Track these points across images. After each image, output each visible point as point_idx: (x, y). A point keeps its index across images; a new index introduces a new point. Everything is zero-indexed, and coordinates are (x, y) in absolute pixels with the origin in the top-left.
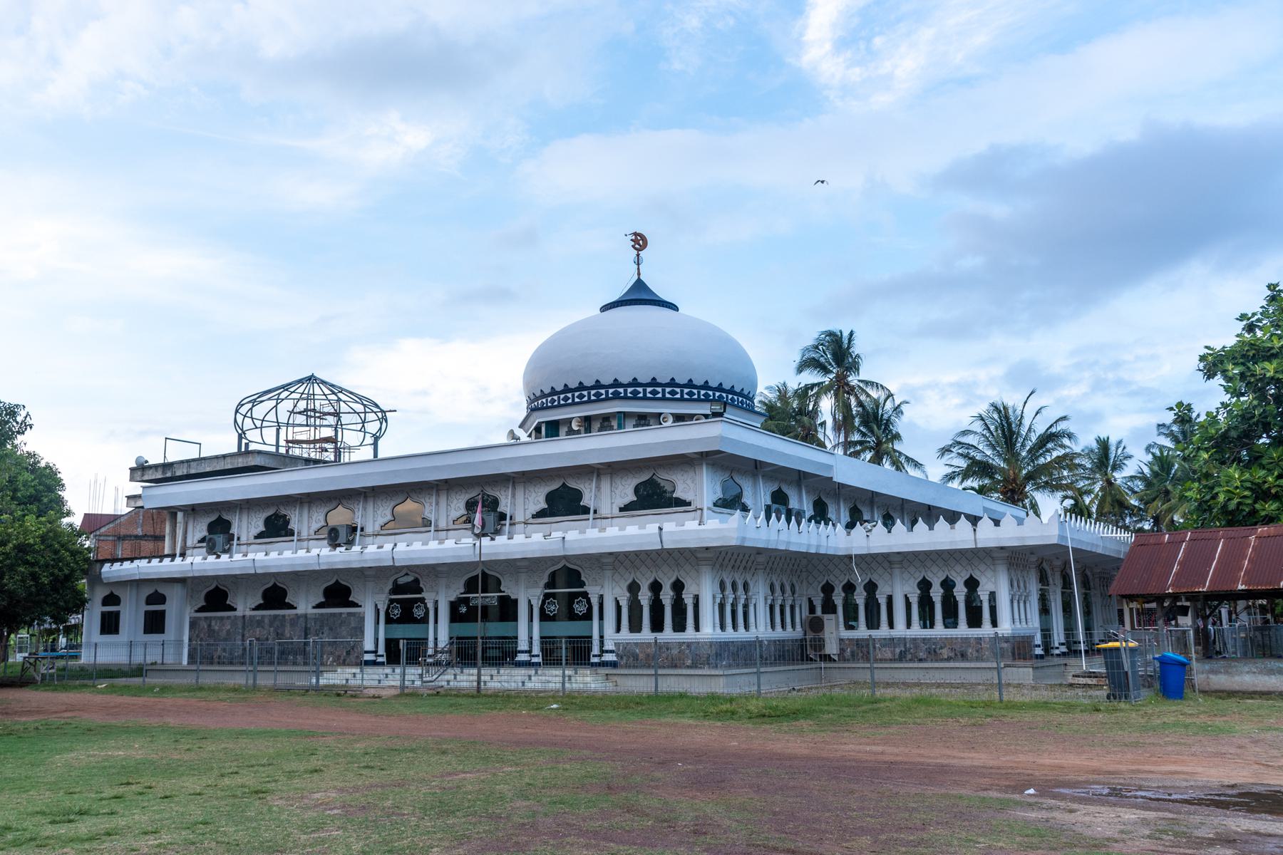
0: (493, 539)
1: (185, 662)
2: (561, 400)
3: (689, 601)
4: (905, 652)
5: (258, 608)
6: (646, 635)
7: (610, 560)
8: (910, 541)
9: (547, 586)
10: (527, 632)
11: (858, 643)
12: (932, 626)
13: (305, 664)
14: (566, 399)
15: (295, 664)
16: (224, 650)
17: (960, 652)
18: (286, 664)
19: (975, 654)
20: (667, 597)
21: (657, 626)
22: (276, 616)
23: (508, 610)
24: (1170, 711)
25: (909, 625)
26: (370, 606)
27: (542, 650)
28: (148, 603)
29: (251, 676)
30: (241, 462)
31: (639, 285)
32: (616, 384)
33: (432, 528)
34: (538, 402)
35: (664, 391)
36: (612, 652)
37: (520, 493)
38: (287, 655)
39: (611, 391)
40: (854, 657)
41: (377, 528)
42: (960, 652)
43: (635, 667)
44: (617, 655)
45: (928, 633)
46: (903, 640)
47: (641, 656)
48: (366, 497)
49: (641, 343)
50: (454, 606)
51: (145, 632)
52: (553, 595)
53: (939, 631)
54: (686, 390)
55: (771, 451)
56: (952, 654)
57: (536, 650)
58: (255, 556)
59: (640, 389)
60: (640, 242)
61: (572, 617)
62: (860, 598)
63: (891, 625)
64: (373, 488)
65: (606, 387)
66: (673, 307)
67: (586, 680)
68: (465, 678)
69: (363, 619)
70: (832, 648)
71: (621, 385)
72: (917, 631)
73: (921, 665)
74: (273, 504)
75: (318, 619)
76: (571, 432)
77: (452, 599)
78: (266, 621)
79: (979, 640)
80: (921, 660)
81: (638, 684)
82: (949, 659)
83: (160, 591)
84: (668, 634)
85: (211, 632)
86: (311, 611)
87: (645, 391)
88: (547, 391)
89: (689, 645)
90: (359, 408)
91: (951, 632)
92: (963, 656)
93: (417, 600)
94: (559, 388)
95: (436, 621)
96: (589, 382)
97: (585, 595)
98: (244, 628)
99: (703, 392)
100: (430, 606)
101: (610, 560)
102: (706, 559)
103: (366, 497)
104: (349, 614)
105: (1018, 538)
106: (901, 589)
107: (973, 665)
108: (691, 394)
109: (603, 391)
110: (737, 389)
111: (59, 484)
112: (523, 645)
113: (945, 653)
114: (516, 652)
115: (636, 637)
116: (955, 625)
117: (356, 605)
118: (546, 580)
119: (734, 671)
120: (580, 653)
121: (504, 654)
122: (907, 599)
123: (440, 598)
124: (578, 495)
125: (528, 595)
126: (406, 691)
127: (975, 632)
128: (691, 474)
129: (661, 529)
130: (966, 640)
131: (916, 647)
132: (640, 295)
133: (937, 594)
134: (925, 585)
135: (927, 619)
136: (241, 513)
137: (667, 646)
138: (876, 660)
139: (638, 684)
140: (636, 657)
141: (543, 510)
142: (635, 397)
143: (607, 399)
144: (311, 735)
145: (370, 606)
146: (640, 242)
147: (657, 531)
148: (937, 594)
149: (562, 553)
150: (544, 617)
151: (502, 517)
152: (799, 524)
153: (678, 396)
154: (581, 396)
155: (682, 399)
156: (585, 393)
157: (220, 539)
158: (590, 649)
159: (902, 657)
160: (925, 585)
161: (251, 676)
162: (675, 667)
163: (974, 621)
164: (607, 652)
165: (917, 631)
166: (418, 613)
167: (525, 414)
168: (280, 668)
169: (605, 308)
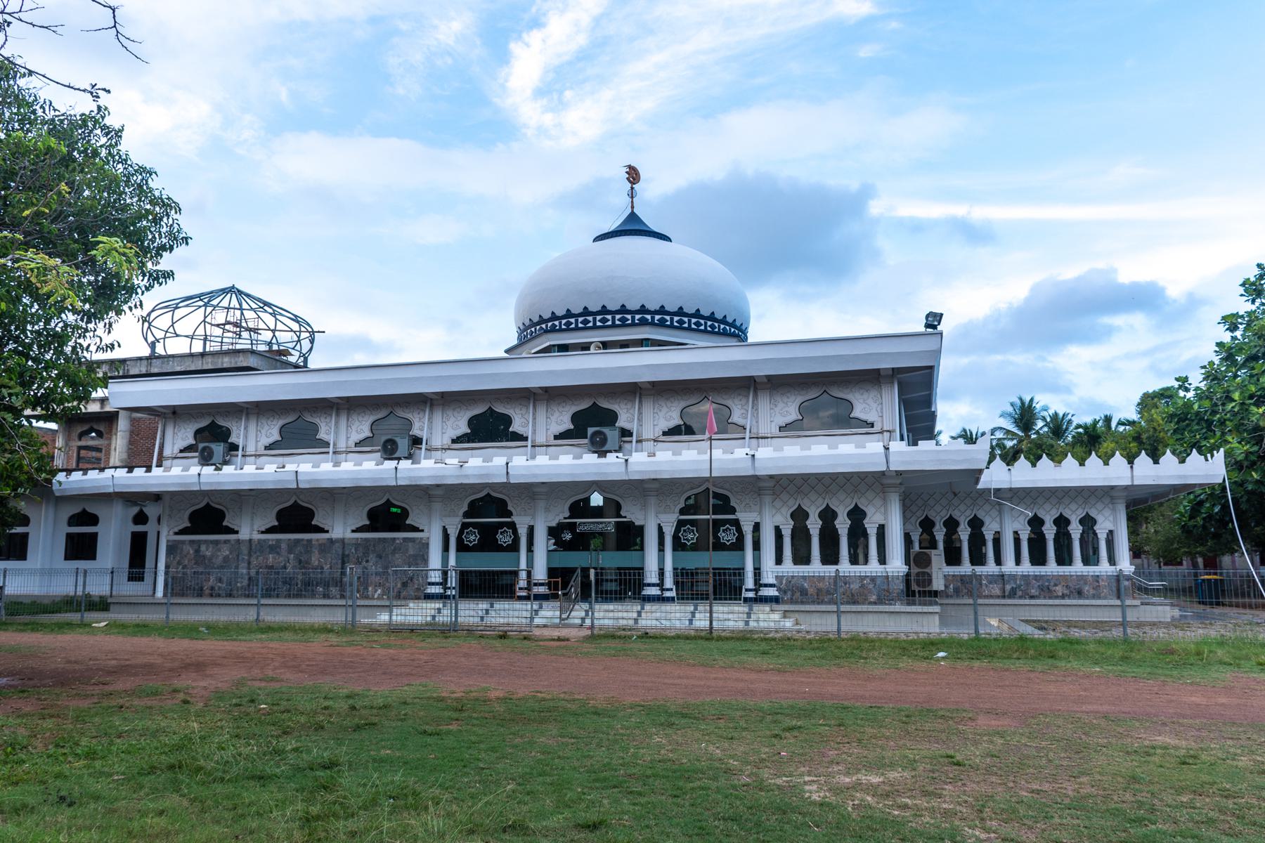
0: (217, 469)
1: (160, 593)
2: (548, 327)
3: (989, 537)
4: (1013, 590)
5: (270, 530)
6: (816, 567)
7: (771, 484)
8: (1058, 477)
10: (656, 562)
11: (963, 579)
12: (866, 562)
13: (343, 597)
15: (326, 596)
16: (220, 580)
17: (1077, 589)
18: (313, 596)
19: (1092, 592)
20: (1075, 530)
22: (298, 541)
23: (630, 537)
25: (1018, 562)
26: (434, 530)
27: (676, 583)
28: (70, 524)
29: (350, 610)
30: (226, 362)
31: (633, 217)
32: (643, 310)
33: (331, 450)
36: (654, 585)
37: (438, 416)
38: (304, 586)
39: (637, 317)
40: (957, 592)
41: (176, 450)
42: (1077, 589)
43: (802, 603)
44: (779, 590)
46: (1013, 577)
47: (811, 591)
48: (432, 406)
51: (66, 559)
52: (693, 523)
53: (1052, 568)
54: (694, 320)
56: (1066, 592)
57: (669, 582)
58: (257, 468)
61: (719, 546)
62: (964, 534)
63: (998, 561)
64: (348, 400)
65: (613, 313)
67: (729, 616)
68: (471, 612)
69: (427, 545)
70: (938, 584)
71: (649, 312)
72: (1027, 568)
73: (1033, 602)
74: (294, 410)
75: (357, 544)
77: (554, 524)
78: (284, 546)
79: (1097, 578)
80: (1032, 597)
81: (820, 622)
82: (1063, 597)
83: (89, 510)
85: (199, 558)
86: (349, 535)
88: (536, 319)
89: (873, 579)
90: (295, 327)
91: (1065, 570)
92: (1080, 594)
94: (560, 313)
95: (530, 549)
98: (250, 555)
101: (771, 484)
103: (432, 406)
104: (405, 539)
105: (1180, 477)
107: (1057, 602)
108: (698, 324)
109: (629, 317)
111: (1163, 290)
112: (651, 577)
113: (1059, 590)
114: (641, 585)
115: (802, 570)
116: (1097, 563)
117: (416, 529)
118: (465, 508)
120: (726, 587)
121: (629, 586)
122: (660, 528)
123: (538, 523)
124: (508, 420)
125: (657, 521)
126: (261, 625)
127: (1091, 570)
128: (874, 393)
129: (887, 449)
130: (1082, 578)
131: (1028, 584)
134: (799, 516)
135: (1038, 557)
136: (247, 419)
137: (846, 580)
138: (980, 597)
139: (820, 622)
140: (804, 592)
141: (466, 435)
142: (662, 324)
143: (633, 325)
145: (434, 530)
146: (633, 175)
147: (882, 450)
148: (814, 525)
149: (750, 473)
150: (678, 545)
151: (234, 447)
154: (568, 324)
156: (590, 318)
157: (218, 449)
158: (742, 582)
159: (1013, 594)
160: (1036, 523)
161: (350, 610)
162: (855, 603)
164: (766, 585)
166: (504, 539)
168: (263, 601)
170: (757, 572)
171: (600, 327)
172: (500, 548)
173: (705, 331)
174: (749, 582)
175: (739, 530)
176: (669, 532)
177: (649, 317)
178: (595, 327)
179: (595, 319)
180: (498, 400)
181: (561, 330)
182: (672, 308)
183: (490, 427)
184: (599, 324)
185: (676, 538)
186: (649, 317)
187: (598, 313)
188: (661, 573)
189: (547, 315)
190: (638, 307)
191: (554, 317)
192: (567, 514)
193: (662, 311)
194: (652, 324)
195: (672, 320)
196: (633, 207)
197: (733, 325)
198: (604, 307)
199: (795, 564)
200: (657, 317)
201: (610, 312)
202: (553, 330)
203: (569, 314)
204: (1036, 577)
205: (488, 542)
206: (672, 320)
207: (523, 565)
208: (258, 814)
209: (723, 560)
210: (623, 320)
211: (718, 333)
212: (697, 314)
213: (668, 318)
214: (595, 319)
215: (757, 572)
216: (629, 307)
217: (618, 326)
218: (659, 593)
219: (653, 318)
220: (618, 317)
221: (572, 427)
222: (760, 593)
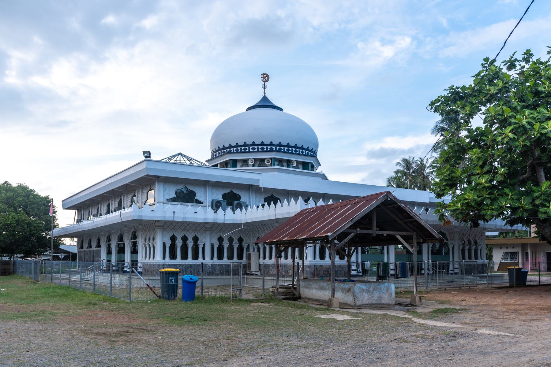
2: (228, 152)
3: (201, 246)
20: (190, 243)
24: (514, 300)
25: (212, 258)
31: (265, 99)
35: (258, 148)
45: (322, 262)
49: (265, 127)
54: (294, 149)
55: (214, 176)
59: (265, 147)
60: (265, 78)
63: (204, 258)
65: (276, 146)
66: (281, 110)
72: (216, 261)
88: (221, 147)
95: (388, 253)
96: (258, 142)
102: (158, 226)
106: (207, 241)
108: (302, 152)
110: (305, 147)
119: (210, 277)
124: (194, 194)
132: (265, 103)
133: (179, 243)
134: (173, 239)
142: (280, 151)
143: (267, 151)
144: (487, 305)
146: (265, 78)
148: (179, 243)
152: (246, 209)
153: (256, 150)
156: (247, 148)
163: (196, 257)
165: (216, 261)
169: (249, 109)
171: (252, 152)
173: (299, 154)
177: (274, 147)
178: (249, 152)
179: (249, 148)
180: (234, 188)
181: (234, 153)
183: (186, 196)
184: (251, 150)
186: (274, 147)
187: (251, 145)
190: (251, 143)
191: (230, 146)
193: (280, 145)
194: (276, 151)
195: (284, 149)
196: (265, 93)
197: (311, 151)
198: (262, 142)
200: (278, 148)
201: (265, 145)
202: (230, 152)
206: (284, 149)
208: (261, 358)
211: (305, 155)
212: (296, 147)
213: (282, 148)
214: (249, 148)
216: (274, 143)
219: (276, 148)
220: (260, 147)
221: (195, 198)
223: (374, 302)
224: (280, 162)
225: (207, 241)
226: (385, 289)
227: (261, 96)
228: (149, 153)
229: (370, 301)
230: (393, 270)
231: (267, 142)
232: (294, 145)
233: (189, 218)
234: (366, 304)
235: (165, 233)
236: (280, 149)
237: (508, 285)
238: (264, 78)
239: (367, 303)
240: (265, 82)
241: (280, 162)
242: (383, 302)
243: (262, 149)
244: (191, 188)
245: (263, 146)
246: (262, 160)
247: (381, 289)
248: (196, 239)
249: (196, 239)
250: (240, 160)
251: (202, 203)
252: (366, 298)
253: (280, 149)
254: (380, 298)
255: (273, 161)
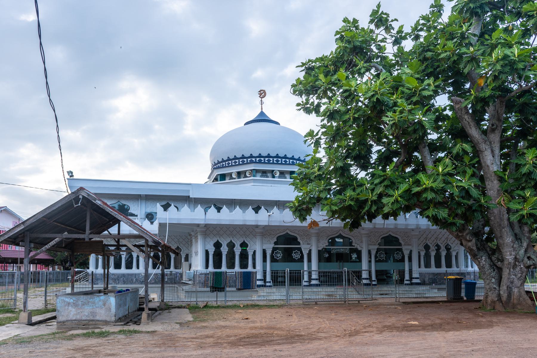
9: (276, 243)
14: (229, 164)
20: (238, 250)
21: (438, 265)
31: (262, 113)
34: (216, 166)
39: (249, 160)
50: (320, 253)
52: (277, 248)
59: (271, 159)
60: (262, 94)
65: (256, 157)
76: (231, 178)
77: (320, 249)
84: (443, 269)
87: (273, 160)
93: (398, 249)
97: (300, 249)
99: (291, 161)
100: (406, 253)
109: (245, 160)
116: (430, 267)
132: (262, 118)
133: (224, 250)
134: (218, 245)
142: (260, 162)
143: (247, 163)
148: (224, 250)
155: (239, 164)
156: (237, 161)
166: (296, 256)
167: (210, 171)
169: (247, 124)
170: (411, 271)
171: (234, 165)
172: (294, 261)
174: (306, 278)
175: (302, 253)
176: (373, 253)
177: (254, 159)
179: (239, 161)
182: (264, 154)
184: (233, 164)
185: (376, 257)
186: (254, 159)
187: (241, 158)
188: (265, 273)
189: (220, 160)
190: (249, 155)
192: (327, 244)
194: (256, 162)
195: (264, 160)
196: (262, 109)
199: (241, 268)
200: (258, 159)
203: (229, 159)
204: (128, 274)
205: (288, 256)
207: (306, 268)
209: (294, 266)
210: (243, 161)
212: (293, 158)
213: (263, 159)
214: (239, 161)
215: (411, 271)
216: (254, 155)
217: (241, 164)
218: (369, 282)
219: (256, 160)
222: (312, 283)
223: (84, 318)
224: (264, 173)
225: (256, 247)
226: (101, 303)
227: (260, 111)
228: (72, 173)
229: (78, 317)
230: (260, 280)
231: (247, 155)
232: (283, 156)
233: (379, 224)
234: (72, 320)
235: (208, 239)
236: (260, 161)
237: (446, 299)
238: (261, 94)
239: (74, 318)
240: (262, 98)
241: (264, 173)
242: (98, 318)
243: (277, 161)
244: (124, 202)
245: (244, 159)
246: (245, 172)
247: (94, 303)
248: (244, 245)
249: (244, 245)
250: (287, 172)
251: (137, 216)
252: (72, 313)
253: (260, 161)
254: (93, 313)
255: (255, 172)
